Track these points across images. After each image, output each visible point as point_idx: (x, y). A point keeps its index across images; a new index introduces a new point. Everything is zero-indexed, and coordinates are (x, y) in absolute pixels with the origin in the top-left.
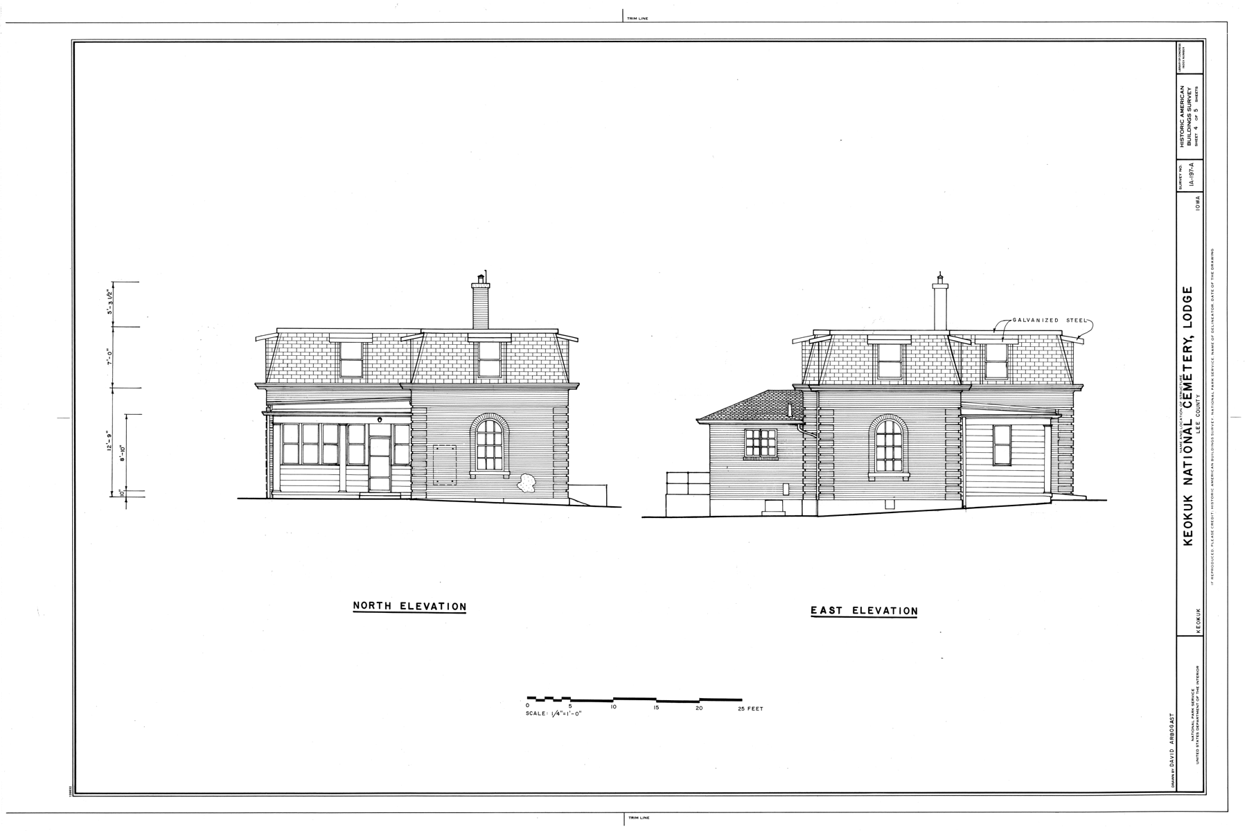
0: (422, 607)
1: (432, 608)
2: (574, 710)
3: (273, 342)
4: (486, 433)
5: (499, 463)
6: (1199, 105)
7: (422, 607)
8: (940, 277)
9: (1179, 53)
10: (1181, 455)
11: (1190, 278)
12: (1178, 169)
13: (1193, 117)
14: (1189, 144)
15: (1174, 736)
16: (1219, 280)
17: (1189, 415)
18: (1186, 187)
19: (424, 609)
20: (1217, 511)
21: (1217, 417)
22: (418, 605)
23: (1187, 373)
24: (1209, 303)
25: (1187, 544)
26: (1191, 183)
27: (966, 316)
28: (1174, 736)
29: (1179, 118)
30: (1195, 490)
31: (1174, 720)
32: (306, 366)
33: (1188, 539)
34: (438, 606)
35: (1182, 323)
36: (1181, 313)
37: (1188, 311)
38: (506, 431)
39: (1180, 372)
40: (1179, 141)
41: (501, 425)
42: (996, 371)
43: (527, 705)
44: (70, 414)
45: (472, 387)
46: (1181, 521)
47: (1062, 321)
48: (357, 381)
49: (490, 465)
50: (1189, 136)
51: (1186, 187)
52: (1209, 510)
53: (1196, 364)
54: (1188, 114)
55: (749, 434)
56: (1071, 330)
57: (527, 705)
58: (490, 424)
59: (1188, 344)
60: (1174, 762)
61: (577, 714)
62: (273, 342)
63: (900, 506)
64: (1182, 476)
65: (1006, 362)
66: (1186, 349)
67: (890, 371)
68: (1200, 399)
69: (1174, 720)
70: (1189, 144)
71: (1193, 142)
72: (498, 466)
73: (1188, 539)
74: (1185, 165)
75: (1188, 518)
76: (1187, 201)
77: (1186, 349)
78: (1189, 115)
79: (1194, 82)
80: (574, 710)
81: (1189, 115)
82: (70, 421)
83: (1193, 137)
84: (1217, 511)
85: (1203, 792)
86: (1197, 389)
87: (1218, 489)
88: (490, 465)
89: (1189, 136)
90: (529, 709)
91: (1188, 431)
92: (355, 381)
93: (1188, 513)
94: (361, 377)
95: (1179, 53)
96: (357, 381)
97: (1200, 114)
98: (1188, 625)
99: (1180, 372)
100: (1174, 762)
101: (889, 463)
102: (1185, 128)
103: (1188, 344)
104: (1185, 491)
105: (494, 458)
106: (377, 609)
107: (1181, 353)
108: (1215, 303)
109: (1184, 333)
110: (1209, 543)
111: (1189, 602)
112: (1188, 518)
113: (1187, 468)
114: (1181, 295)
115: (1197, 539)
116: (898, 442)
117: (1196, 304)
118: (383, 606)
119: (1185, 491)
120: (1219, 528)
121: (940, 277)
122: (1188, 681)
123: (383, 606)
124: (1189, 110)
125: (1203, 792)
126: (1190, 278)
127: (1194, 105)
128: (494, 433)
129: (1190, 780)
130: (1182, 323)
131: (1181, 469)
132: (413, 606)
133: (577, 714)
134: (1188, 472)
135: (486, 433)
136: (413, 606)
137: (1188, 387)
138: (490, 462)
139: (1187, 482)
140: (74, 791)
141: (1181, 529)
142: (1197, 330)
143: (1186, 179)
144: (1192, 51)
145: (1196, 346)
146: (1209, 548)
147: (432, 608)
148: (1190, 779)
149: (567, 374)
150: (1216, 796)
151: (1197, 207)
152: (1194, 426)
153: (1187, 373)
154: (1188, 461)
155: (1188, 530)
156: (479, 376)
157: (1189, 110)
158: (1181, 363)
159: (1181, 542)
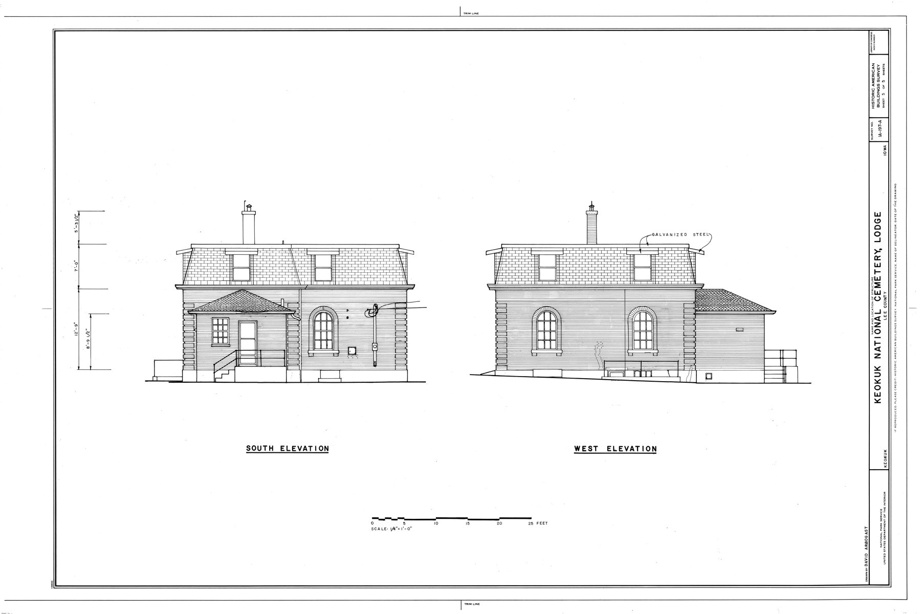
0: (623, 449)
1: (305, 450)
2: (406, 526)
3: (499, 254)
4: (544, 321)
5: (650, 344)
6: (885, 78)
7: (623, 449)
8: (592, 206)
9: (871, 38)
10: (873, 336)
11: (879, 205)
12: (870, 125)
13: (881, 87)
14: (878, 106)
15: (867, 544)
16: (900, 207)
17: (878, 306)
18: (876, 138)
19: (624, 451)
20: (899, 378)
21: (899, 308)
22: (293, 447)
23: (877, 275)
24: (893, 224)
25: (877, 402)
26: (880, 135)
27: (269, 230)
28: (867, 544)
29: (871, 87)
30: (882, 363)
31: (868, 532)
32: (517, 271)
33: (877, 398)
34: (635, 449)
35: (873, 238)
36: (873, 231)
37: (878, 228)
38: (655, 322)
39: (872, 275)
40: (871, 104)
41: (651, 316)
42: (548, 275)
43: (372, 523)
44: (52, 306)
45: (534, 288)
46: (873, 384)
47: (690, 235)
48: (328, 283)
49: (547, 346)
50: (878, 100)
51: (876, 138)
52: (893, 377)
53: (884, 269)
54: (878, 82)
55: (215, 322)
56: (696, 244)
57: (372, 523)
58: (547, 314)
59: (878, 254)
60: (868, 563)
61: (409, 529)
62: (499, 254)
63: (537, 373)
64: (873, 352)
65: (539, 268)
66: (877, 258)
67: (643, 275)
68: (887, 295)
69: (868, 532)
70: (878, 106)
71: (881, 105)
72: (553, 346)
73: (877, 398)
74: (875, 122)
75: (877, 382)
76: (877, 148)
77: (877, 258)
78: (878, 85)
79: (881, 61)
80: (406, 526)
81: (878, 85)
82: (52, 311)
83: (881, 101)
84: (899, 377)
85: (889, 585)
86: (884, 287)
87: (900, 361)
88: (547, 346)
89: (878, 100)
90: (374, 526)
91: (878, 319)
92: (326, 283)
93: (877, 379)
94: (555, 281)
95: (871, 38)
96: (328, 283)
97: (886, 84)
98: (878, 461)
99: (872, 275)
100: (868, 563)
101: (547, 343)
102: (876, 94)
103: (878, 254)
104: (875, 363)
105: (550, 340)
106: (263, 450)
107: (873, 261)
108: (897, 224)
109: (877, 246)
110: (893, 401)
111: (879, 445)
112: (877, 382)
113: (877, 346)
114: (873, 218)
115: (884, 398)
116: (649, 327)
117: (884, 224)
118: (267, 448)
119: (875, 363)
120: (900, 390)
121: (592, 206)
122: (878, 503)
123: (267, 448)
124: (878, 81)
125: (889, 585)
126: (879, 205)
127: (882, 78)
128: (646, 321)
129: (879, 576)
130: (873, 238)
131: (873, 347)
132: (617, 448)
133: (409, 529)
134: (878, 349)
135: (544, 321)
136: (617, 448)
137: (878, 286)
138: (643, 343)
139: (877, 356)
140: (55, 585)
141: (873, 391)
142: (884, 245)
143: (876, 132)
144: (881, 37)
145: (883, 255)
146: (893, 405)
147: (305, 450)
148: (879, 575)
149: (405, 276)
150: (898, 588)
151: (885, 153)
152: (882, 315)
153: (877, 275)
154: (877, 340)
155: (877, 392)
156: (634, 280)
157: (878, 81)
158: (872, 268)
159: (872, 401)
